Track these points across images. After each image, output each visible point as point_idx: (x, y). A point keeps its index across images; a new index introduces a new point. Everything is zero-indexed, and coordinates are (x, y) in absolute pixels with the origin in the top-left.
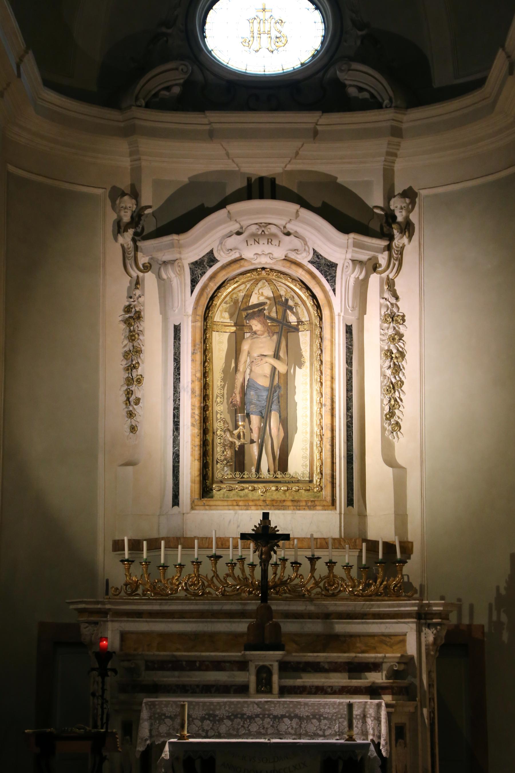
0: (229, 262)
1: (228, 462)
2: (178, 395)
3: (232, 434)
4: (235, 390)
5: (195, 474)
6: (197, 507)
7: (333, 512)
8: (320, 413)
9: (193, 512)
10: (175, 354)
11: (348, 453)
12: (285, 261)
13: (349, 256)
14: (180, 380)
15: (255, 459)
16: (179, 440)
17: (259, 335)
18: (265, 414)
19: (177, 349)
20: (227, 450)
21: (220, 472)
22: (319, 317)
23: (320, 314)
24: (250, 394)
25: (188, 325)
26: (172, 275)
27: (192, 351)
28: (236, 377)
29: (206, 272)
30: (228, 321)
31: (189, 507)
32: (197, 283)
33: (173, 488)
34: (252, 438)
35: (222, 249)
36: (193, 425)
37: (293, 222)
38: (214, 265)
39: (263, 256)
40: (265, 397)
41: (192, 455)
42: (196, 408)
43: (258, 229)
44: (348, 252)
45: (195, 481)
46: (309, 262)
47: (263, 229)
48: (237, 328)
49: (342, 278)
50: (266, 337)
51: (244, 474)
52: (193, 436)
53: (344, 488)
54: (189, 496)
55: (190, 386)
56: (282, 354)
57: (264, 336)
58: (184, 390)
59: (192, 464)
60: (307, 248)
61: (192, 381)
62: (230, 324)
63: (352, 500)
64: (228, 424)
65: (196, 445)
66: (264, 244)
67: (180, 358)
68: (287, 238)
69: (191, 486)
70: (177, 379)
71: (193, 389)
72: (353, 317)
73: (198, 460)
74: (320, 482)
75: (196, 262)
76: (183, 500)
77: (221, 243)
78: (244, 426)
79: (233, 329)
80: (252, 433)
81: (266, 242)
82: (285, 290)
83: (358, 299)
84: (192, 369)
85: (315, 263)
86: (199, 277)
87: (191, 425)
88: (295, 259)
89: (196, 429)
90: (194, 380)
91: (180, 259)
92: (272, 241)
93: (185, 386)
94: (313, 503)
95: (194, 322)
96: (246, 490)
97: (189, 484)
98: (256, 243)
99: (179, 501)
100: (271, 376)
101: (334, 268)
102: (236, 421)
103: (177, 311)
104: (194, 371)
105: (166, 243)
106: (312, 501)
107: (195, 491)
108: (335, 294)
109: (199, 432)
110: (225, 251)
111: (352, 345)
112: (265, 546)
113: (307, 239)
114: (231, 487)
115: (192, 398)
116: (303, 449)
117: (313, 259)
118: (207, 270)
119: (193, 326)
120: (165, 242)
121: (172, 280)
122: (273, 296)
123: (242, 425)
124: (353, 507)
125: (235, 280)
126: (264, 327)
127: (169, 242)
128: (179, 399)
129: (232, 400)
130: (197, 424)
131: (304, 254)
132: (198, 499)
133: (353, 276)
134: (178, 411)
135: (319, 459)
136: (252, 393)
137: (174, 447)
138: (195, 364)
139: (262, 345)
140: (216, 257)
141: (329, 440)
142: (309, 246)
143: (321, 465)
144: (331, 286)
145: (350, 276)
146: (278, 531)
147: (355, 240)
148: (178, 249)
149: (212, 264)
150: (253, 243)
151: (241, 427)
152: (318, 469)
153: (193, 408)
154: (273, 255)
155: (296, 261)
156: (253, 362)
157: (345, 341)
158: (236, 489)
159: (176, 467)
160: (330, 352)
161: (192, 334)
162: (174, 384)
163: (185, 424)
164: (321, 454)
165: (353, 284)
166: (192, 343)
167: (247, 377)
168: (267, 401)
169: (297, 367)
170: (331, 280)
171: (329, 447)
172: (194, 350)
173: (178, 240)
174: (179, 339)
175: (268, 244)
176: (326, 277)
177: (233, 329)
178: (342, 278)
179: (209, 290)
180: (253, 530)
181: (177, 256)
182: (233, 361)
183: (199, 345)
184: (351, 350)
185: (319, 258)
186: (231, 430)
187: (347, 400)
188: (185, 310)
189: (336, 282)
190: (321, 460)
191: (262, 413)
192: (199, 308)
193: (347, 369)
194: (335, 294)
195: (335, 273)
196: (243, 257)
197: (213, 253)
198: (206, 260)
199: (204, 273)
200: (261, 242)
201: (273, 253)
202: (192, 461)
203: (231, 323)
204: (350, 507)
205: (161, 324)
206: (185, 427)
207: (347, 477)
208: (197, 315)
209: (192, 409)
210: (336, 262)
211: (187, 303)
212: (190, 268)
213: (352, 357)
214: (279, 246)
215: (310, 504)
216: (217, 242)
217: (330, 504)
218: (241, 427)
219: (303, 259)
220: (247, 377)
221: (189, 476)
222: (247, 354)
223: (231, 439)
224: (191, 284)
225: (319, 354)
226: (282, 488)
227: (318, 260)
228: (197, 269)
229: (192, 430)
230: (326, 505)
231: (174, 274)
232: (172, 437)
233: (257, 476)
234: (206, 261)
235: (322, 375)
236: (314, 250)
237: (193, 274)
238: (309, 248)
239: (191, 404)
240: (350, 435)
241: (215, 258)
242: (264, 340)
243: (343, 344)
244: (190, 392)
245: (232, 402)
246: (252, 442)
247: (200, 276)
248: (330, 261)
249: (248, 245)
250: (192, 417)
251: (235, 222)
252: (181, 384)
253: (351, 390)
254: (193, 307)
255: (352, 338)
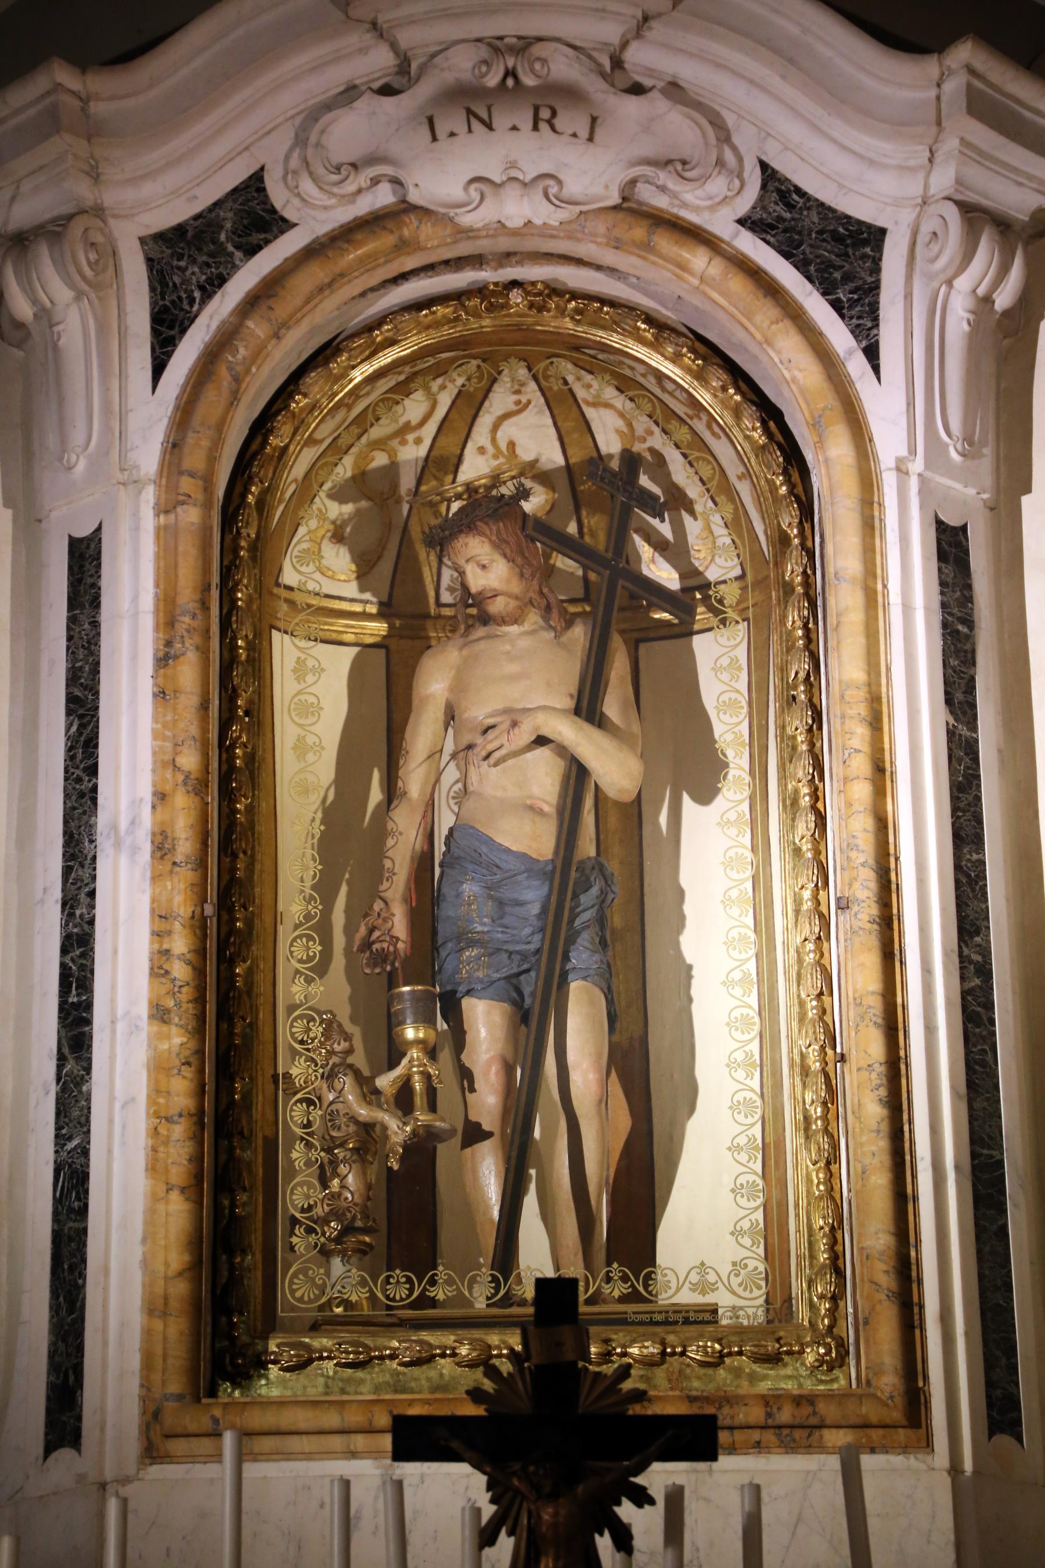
0: (342, 226)
1: (348, 1230)
2: (85, 874)
3: (370, 1093)
4: (386, 885)
5: (167, 1264)
6: (178, 1446)
7: (913, 1461)
8: (818, 963)
9: (155, 1471)
10: (73, 677)
11: (978, 1149)
12: (620, 215)
13: (943, 180)
14: (94, 801)
15: (492, 1220)
16: (88, 1100)
17: (503, 621)
18: (533, 994)
19: (81, 653)
20: (343, 1169)
21: (304, 1271)
22: (798, 500)
23: (799, 490)
24: (459, 895)
25: (136, 529)
26: (60, 292)
27: (156, 651)
28: (390, 825)
29: (230, 275)
30: (351, 590)
31: (133, 1447)
32: (183, 331)
33: (52, 1355)
34: (473, 1117)
35: (307, 164)
36: (159, 1014)
37: (657, 30)
38: (267, 242)
39: (512, 192)
40: (535, 909)
41: (153, 1168)
42: (177, 926)
43: (485, 62)
44: (939, 157)
45: (166, 1303)
46: (741, 222)
47: (510, 63)
48: (391, 627)
49: (908, 296)
50: (532, 633)
51: (433, 1282)
52: (158, 1067)
53: (967, 1334)
54: (134, 1385)
55: (147, 819)
56: (611, 708)
57: (527, 627)
58: (117, 845)
59: (151, 1213)
60: (729, 156)
61: (155, 794)
62: (358, 608)
63: (1012, 1403)
64: (348, 1038)
65: (174, 1111)
66: (514, 128)
67: (97, 694)
68: (632, 105)
69: (148, 1333)
70: (82, 795)
71: (163, 833)
72: (972, 491)
73: (183, 1190)
74: (833, 1312)
75: (180, 230)
76: (103, 1410)
77: (301, 140)
78: (432, 1053)
79: (378, 628)
80: (472, 1090)
81: (525, 120)
82: (620, 423)
83: (992, 404)
84: (156, 735)
85: (772, 227)
86: (192, 301)
87: (152, 1017)
88: (675, 210)
89: (174, 1029)
90: (168, 788)
91: (98, 211)
92: (554, 114)
93: (123, 825)
94: (807, 1410)
95: (167, 512)
96: (445, 1365)
97: (137, 1319)
98: (476, 125)
99: (79, 1418)
100: (560, 811)
101: (868, 250)
102: (392, 1023)
103: (81, 467)
104: (169, 745)
105: (22, 118)
106: (799, 1400)
107: (165, 1357)
108: (876, 369)
109: (193, 1045)
110: (321, 171)
111: (969, 622)
112: (553, 1497)
113: (730, 119)
114: (365, 1346)
115: (155, 878)
116: (739, 1148)
117: (764, 208)
118: (235, 268)
119: (166, 527)
120: (17, 112)
121: (56, 318)
122: (560, 461)
123: (418, 1042)
124: (1020, 1440)
125: (378, 336)
126: (522, 575)
127: (32, 112)
128: (92, 894)
129: (371, 931)
130: (178, 1005)
131: (718, 185)
132: (180, 1397)
133: (964, 283)
134: (83, 955)
135: (820, 1198)
136: (469, 889)
137: (60, 1139)
138: (175, 709)
139: (512, 668)
140: (278, 206)
141: (877, 1074)
142: (742, 149)
143: (833, 1229)
144: (857, 332)
145: (949, 283)
146: (639, 1396)
147: (978, 84)
148: (81, 146)
149: (256, 238)
150: (461, 127)
151: (414, 1053)
152: (822, 1245)
153: (164, 926)
154: (560, 183)
155: (678, 217)
156: (470, 747)
157: (936, 599)
158: (392, 1357)
159: (71, 1239)
160: (861, 640)
161: (157, 569)
162: (66, 822)
163: (120, 1012)
164: (834, 1168)
165: (966, 328)
166: (157, 610)
167: (445, 821)
168: (542, 930)
169: (686, 799)
170: (853, 303)
171: (874, 1111)
172: (168, 644)
173: (85, 101)
174: (96, 603)
175: (536, 128)
176: (827, 290)
177: (378, 628)
178: (908, 296)
179: (242, 352)
180: (476, 1395)
181: (83, 191)
182: (376, 776)
183: (194, 616)
184: (968, 647)
185: (790, 206)
186: (366, 1072)
187: (957, 882)
188: (122, 455)
189: (882, 313)
190: (833, 1198)
191: (518, 990)
192: (191, 438)
193: (951, 733)
194: (876, 369)
195: (876, 270)
196: (414, 197)
197: (262, 190)
198: (228, 219)
199: (221, 281)
200: (501, 121)
201: (561, 177)
202: (154, 1199)
203: (367, 602)
204: (1004, 1440)
205: (8, 549)
206: (120, 1027)
207: (981, 1277)
208: (181, 473)
209: (158, 935)
210: (880, 223)
211: (134, 423)
212: (149, 261)
213: (972, 680)
214: (591, 139)
215: (785, 1415)
216: (285, 138)
217: (896, 1415)
218: (414, 1053)
219: (712, 208)
220: (445, 821)
221: (137, 1278)
222: (440, 715)
223: (363, 1112)
224: (155, 332)
225: (802, 675)
226: (634, 1350)
227: (788, 215)
228: (182, 264)
229: (154, 1039)
230: (874, 1419)
231: (71, 285)
232: (53, 1089)
233: (497, 1289)
234: (228, 225)
235: (822, 778)
236: (764, 166)
237: (164, 284)
238: (740, 159)
239: (153, 911)
240: (983, 1064)
241: (273, 211)
242: (524, 643)
243: (927, 609)
244: (147, 848)
245: (367, 945)
246: (474, 1134)
247: (197, 294)
248: (848, 217)
249: (434, 139)
250: (158, 971)
251: (369, 37)
252: (102, 819)
253: (978, 841)
254: (166, 440)
255: (969, 587)
